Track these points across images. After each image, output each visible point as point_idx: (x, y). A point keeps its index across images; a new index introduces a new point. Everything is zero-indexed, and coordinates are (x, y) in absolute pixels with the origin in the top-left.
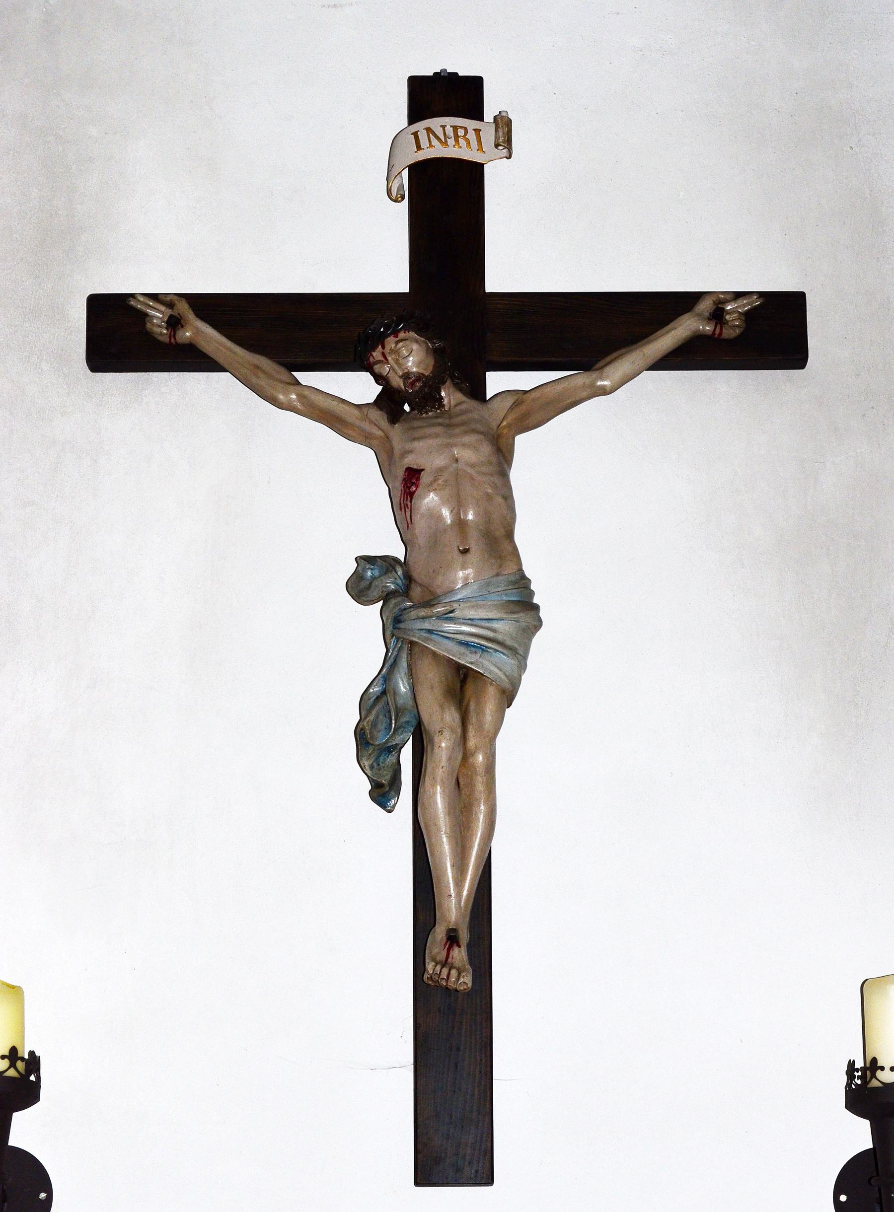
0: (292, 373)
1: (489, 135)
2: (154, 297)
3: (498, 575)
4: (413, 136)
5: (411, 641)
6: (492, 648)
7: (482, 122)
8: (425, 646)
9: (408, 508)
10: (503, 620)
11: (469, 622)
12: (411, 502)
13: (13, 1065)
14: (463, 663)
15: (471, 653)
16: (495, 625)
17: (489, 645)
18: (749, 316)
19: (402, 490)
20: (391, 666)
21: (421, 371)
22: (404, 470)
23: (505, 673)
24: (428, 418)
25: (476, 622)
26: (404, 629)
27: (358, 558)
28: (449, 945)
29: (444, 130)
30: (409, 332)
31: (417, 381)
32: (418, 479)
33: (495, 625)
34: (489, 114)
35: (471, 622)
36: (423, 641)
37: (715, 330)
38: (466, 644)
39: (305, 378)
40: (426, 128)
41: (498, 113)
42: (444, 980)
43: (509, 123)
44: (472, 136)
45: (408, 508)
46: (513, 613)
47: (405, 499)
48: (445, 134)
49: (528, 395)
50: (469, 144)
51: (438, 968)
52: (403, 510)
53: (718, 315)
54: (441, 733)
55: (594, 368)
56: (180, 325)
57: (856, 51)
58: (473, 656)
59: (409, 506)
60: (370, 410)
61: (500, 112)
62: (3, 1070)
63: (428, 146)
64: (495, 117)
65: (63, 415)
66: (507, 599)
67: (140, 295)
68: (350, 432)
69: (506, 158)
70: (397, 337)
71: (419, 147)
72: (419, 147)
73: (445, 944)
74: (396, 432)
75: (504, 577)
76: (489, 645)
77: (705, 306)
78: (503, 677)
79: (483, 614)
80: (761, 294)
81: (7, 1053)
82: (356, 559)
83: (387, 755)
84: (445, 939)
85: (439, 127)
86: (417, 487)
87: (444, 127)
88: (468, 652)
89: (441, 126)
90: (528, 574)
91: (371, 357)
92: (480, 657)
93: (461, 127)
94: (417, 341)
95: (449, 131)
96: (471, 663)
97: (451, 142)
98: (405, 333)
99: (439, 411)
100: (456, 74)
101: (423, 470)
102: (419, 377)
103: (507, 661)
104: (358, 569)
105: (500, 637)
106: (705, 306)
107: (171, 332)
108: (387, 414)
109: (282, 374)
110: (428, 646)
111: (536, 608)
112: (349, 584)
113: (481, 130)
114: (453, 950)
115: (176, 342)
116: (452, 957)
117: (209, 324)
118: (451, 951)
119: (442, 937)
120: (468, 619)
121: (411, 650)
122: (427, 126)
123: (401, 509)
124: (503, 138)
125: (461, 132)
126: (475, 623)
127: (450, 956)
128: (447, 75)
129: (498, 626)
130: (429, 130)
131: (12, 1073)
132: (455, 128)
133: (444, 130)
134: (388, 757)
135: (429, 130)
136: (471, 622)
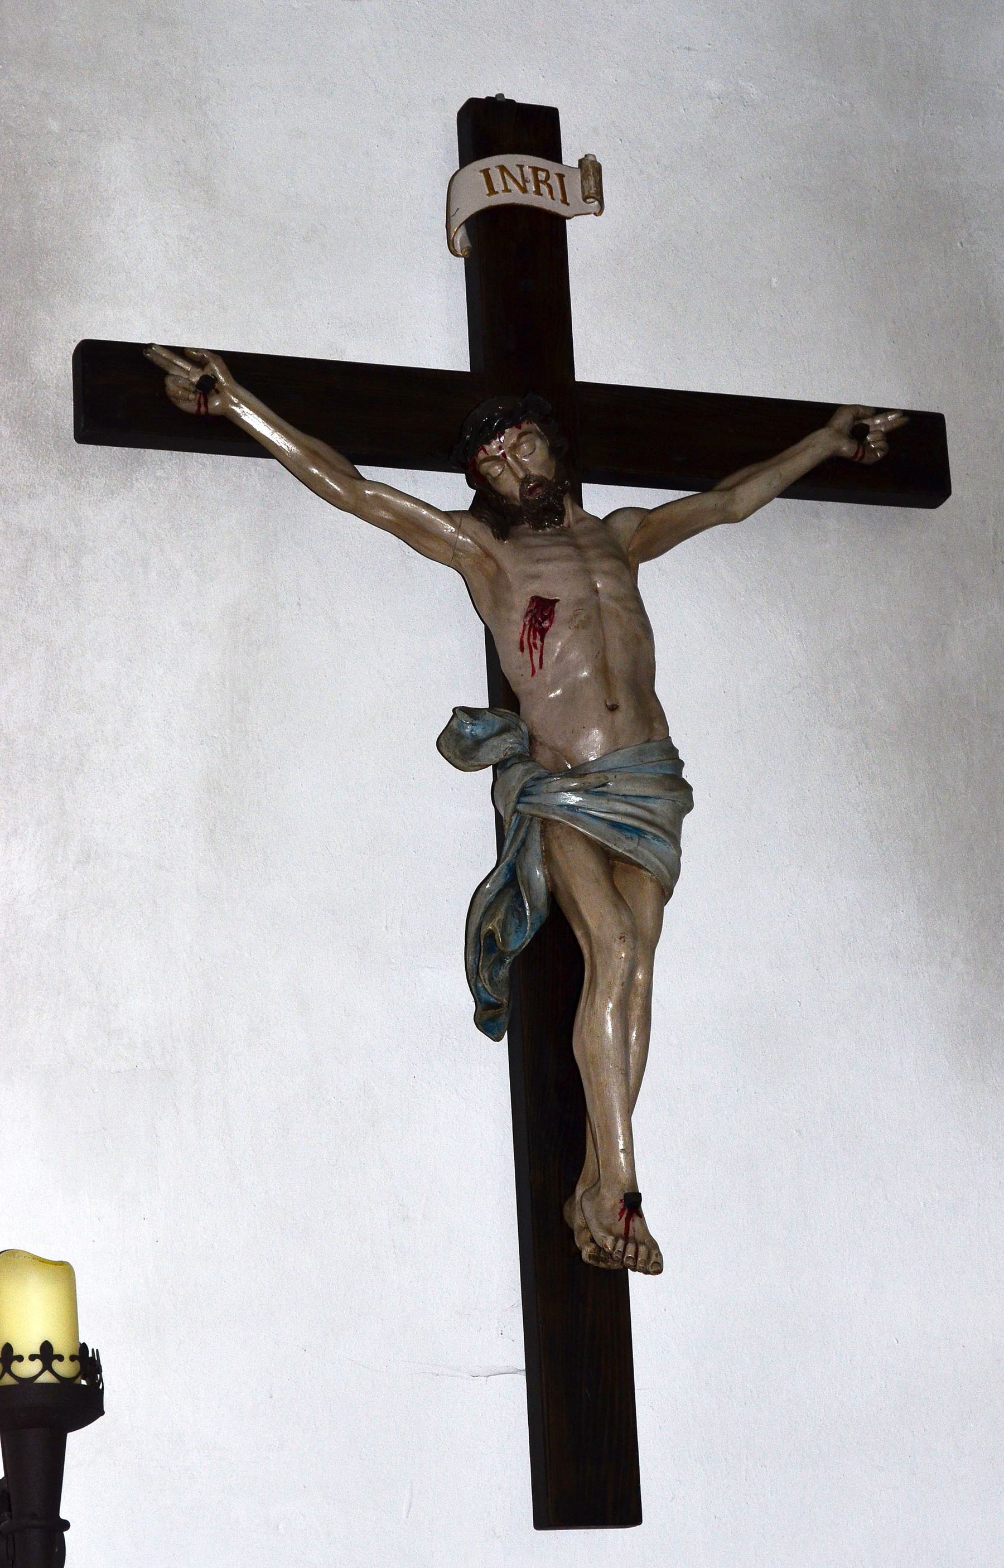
0: (355, 466)
1: (574, 187)
2: (180, 352)
3: (648, 741)
4: (482, 174)
5: (544, 819)
6: (652, 833)
7: (559, 164)
8: (572, 828)
9: (536, 648)
10: (661, 798)
11: (623, 799)
12: (542, 640)
13: (47, 1367)
14: (620, 851)
15: (627, 838)
16: (651, 804)
17: (648, 828)
18: (891, 436)
19: (525, 625)
20: (518, 851)
21: (544, 474)
22: (529, 600)
23: (667, 867)
24: (545, 535)
25: (630, 800)
26: (537, 804)
27: (457, 709)
28: (627, 1214)
29: (522, 171)
30: (531, 423)
31: (538, 487)
32: (552, 612)
33: (651, 804)
34: (570, 157)
35: (625, 798)
36: (568, 820)
37: (857, 452)
38: (614, 824)
39: (367, 472)
40: (499, 166)
41: (584, 156)
42: (631, 1260)
43: (598, 169)
44: (554, 181)
45: (536, 648)
46: (671, 790)
47: (532, 637)
48: (523, 176)
49: (651, 516)
50: (551, 192)
51: (621, 1243)
52: (527, 651)
53: (858, 432)
54: (623, 940)
55: (718, 487)
56: (213, 390)
57: (961, 127)
58: (630, 842)
59: (539, 646)
60: (464, 520)
61: (586, 156)
62: (55, 1371)
63: (503, 189)
64: (580, 161)
65: (30, 497)
66: (662, 771)
67: (160, 347)
68: (433, 545)
69: (595, 214)
70: (520, 428)
71: (492, 191)
72: (492, 191)
73: (621, 1214)
74: (503, 552)
75: (654, 744)
76: (648, 828)
77: (842, 421)
78: (666, 872)
79: (638, 789)
80: (905, 413)
81: (37, 1351)
82: (454, 710)
83: (499, 967)
84: (621, 1206)
85: (495, 169)
86: (551, 622)
87: (521, 167)
88: (623, 838)
89: (518, 165)
90: (675, 743)
91: (482, 451)
92: (638, 844)
93: (543, 170)
94: (541, 437)
95: (528, 172)
96: (630, 852)
97: (531, 187)
98: (528, 423)
99: (558, 527)
100: (514, 101)
101: (557, 601)
102: (541, 482)
103: (665, 848)
104: (451, 724)
105: (658, 820)
106: (842, 421)
107: (200, 397)
108: (492, 527)
109: (342, 463)
110: (576, 827)
111: (687, 788)
112: (442, 742)
113: (564, 176)
114: (633, 1221)
115: (207, 412)
116: (634, 1229)
117: (252, 393)
118: (631, 1221)
119: (615, 1205)
120: (622, 795)
121: (543, 833)
122: (501, 163)
123: (522, 649)
124: (595, 189)
125: (542, 176)
126: (628, 801)
127: (631, 1228)
128: (504, 100)
129: (655, 806)
130: (503, 169)
131: (47, 1378)
132: (535, 170)
133: (522, 171)
134: (500, 969)
135: (503, 169)
136: (625, 798)
